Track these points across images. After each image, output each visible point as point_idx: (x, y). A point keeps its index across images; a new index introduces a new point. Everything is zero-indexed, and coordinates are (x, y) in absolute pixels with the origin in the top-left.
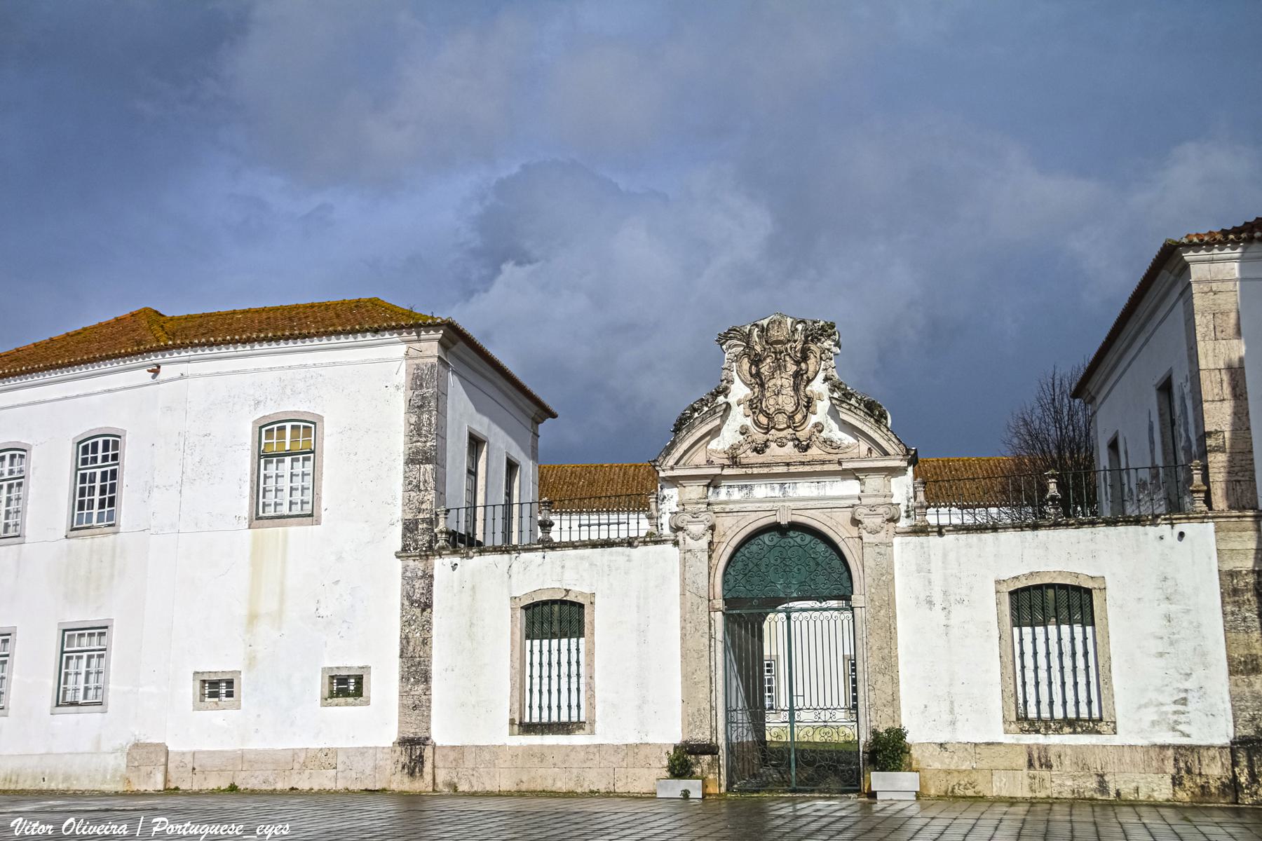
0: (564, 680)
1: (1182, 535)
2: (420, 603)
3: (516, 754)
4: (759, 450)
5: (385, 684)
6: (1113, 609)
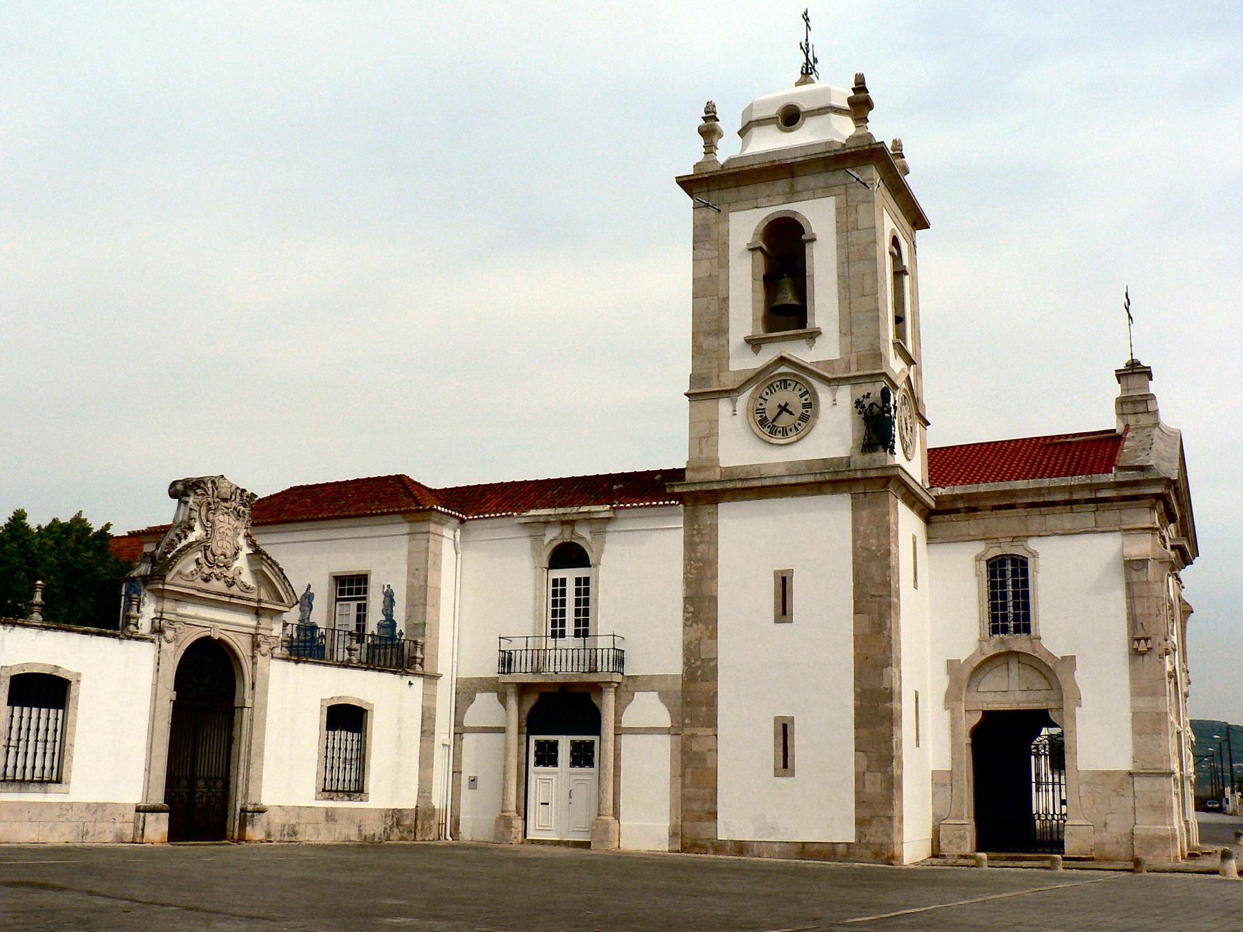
4: (206, 580)
6: (84, 700)
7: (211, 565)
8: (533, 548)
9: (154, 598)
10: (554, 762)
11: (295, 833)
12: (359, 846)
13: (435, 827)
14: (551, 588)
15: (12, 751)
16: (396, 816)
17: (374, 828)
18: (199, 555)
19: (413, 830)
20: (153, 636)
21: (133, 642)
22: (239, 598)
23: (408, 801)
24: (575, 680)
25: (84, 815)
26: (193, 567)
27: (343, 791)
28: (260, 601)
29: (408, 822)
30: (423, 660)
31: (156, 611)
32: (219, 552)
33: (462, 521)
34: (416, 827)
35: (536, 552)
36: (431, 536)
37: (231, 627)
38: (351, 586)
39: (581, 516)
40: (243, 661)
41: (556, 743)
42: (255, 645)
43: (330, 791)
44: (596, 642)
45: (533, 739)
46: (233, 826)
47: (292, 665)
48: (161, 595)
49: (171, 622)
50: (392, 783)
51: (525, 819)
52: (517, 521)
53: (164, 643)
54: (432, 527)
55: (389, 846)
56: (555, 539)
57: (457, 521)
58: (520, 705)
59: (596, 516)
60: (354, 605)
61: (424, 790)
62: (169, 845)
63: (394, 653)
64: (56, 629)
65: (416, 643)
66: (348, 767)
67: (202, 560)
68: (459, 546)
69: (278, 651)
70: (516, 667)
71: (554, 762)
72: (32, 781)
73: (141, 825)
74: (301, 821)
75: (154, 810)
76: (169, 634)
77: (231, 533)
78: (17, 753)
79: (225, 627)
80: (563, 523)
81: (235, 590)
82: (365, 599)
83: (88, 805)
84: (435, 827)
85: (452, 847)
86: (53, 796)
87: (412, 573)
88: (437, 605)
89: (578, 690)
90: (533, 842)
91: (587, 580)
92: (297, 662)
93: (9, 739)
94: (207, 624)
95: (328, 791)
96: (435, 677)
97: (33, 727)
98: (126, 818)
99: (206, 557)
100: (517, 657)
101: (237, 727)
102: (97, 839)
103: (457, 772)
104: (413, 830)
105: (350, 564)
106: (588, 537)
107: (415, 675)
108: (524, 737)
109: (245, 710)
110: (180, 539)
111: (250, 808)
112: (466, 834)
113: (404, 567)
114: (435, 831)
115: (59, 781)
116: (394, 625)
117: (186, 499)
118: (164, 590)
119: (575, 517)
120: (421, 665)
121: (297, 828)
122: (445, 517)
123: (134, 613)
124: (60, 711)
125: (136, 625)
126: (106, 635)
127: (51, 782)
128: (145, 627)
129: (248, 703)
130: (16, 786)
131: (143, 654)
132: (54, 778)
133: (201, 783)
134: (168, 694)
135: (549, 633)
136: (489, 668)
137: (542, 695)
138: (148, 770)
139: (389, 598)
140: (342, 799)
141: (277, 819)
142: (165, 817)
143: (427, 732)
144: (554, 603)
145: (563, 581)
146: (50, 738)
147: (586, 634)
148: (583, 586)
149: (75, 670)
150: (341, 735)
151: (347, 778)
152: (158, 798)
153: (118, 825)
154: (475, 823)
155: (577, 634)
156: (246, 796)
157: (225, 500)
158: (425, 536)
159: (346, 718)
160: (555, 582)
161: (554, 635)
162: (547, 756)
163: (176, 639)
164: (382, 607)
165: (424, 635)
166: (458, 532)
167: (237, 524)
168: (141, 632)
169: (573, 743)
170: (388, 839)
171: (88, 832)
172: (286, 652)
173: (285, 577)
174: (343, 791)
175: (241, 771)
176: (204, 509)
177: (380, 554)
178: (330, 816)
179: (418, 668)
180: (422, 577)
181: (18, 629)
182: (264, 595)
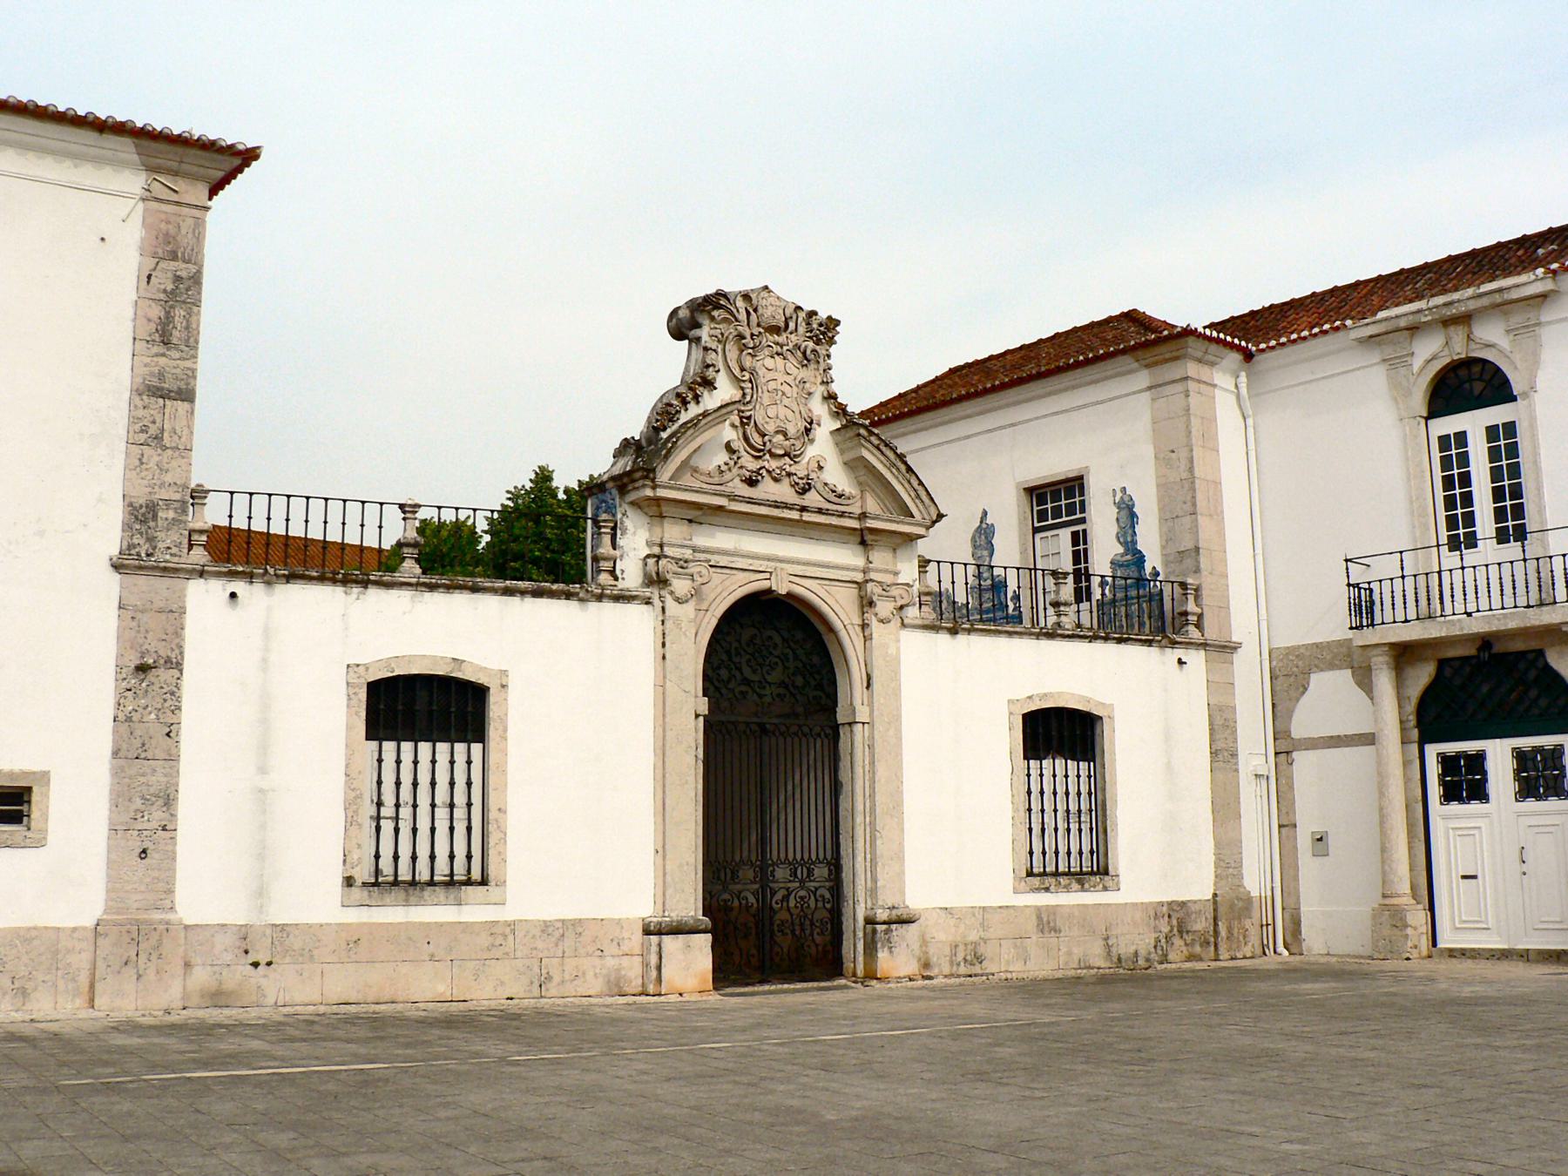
0: (442, 813)
1: (233, 595)
2: (150, 670)
3: (353, 942)
4: (751, 482)
5: (77, 808)
6: (515, 718)
7: (758, 453)
8: (1394, 385)
9: (644, 520)
10: (1478, 792)
11: (979, 959)
12: (1103, 980)
13: (1254, 933)
14: (1437, 455)
15: (387, 827)
16: (1177, 915)
17: (1136, 940)
18: (729, 433)
19: (1212, 940)
20: (647, 592)
21: (608, 607)
22: (820, 511)
23: (1198, 886)
24: (1512, 624)
25: (540, 945)
26: (722, 457)
27: (1068, 874)
28: (863, 516)
29: (1201, 924)
30: (1200, 616)
31: (649, 544)
32: (770, 428)
33: (1248, 356)
34: (1216, 933)
35: (1399, 391)
36: (1191, 385)
37: (810, 571)
38: (1057, 501)
39: (1485, 301)
40: (843, 634)
41: (1480, 757)
42: (867, 603)
43: (1044, 874)
44: (1545, 546)
45: (1432, 750)
46: (853, 949)
47: (943, 638)
48: (657, 510)
49: (682, 563)
50: (1163, 847)
51: (1432, 908)
52: (1354, 334)
53: (669, 601)
54: (1192, 369)
55: (1161, 977)
56: (1434, 358)
57: (1236, 357)
58: (1401, 699)
59: (1515, 295)
60: (1065, 535)
61: (1228, 862)
62: (714, 998)
63: (1146, 609)
64: (449, 588)
65: (1183, 585)
66: (1074, 827)
67: (739, 444)
68: (1247, 404)
69: (912, 613)
70: (1383, 613)
71: (1478, 792)
72: (431, 883)
73: (654, 960)
74: (991, 933)
75: (678, 930)
76: (680, 586)
77: (792, 392)
78: (397, 830)
79: (799, 570)
80: (1447, 322)
81: (812, 499)
82: (1083, 521)
83: (546, 926)
84: (1254, 933)
85: (1290, 973)
86: (474, 910)
87: (1165, 457)
88: (1217, 514)
89: (1519, 646)
90: (1452, 953)
91: (1510, 429)
92: (954, 631)
93: (379, 804)
94: (757, 565)
95: (1039, 873)
96: (1228, 648)
97: (424, 779)
98: (625, 948)
99: (746, 439)
100: (1383, 593)
101: (844, 764)
102: (570, 989)
103: (1287, 826)
104: (1212, 940)
105: (1051, 466)
106: (1504, 342)
107: (1189, 645)
108: (1415, 748)
109: (858, 728)
110: (685, 403)
111: (882, 915)
112: (1315, 941)
113: (1148, 451)
114: (1254, 939)
115: (484, 882)
116: (1140, 559)
117: (694, 333)
118: (658, 501)
119: (1472, 305)
120: (1199, 626)
121: (981, 950)
122: (1213, 347)
123: (605, 549)
124: (476, 748)
125: (612, 572)
126: (552, 594)
127: (469, 882)
128: (631, 575)
129: (862, 714)
130: (398, 893)
131: (636, 622)
132: (476, 874)
133: (781, 873)
134: (691, 702)
135: (1444, 540)
136: (1330, 622)
137: (1442, 663)
138: (662, 851)
139: (1128, 513)
140: (1067, 888)
141: (942, 935)
142: (705, 940)
143: (1223, 753)
144: (1450, 503)
145: (1461, 438)
146: (460, 799)
147: (1521, 534)
148: (1504, 441)
149: (494, 664)
150: (1054, 767)
151: (1074, 850)
152: (689, 905)
153: (611, 962)
154: (1333, 919)
155: (1502, 537)
156: (873, 892)
157: (775, 330)
158: (1179, 387)
159: (1061, 733)
160: (1444, 442)
161: (1454, 544)
162: (1465, 782)
163: (697, 593)
164: (1114, 529)
165: (1197, 570)
166: (1243, 378)
167: (804, 373)
168: (621, 584)
169: (1521, 757)
170: (1164, 959)
171: (549, 978)
172: (929, 614)
173: (909, 469)
174: (1068, 874)
175: (860, 844)
176: (732, 353)
177: (1101, 437)
178: (1047, 922)
179: (1194, 633)
180: (1184, 464)
181: (373, 593)
182: (872, 506)
